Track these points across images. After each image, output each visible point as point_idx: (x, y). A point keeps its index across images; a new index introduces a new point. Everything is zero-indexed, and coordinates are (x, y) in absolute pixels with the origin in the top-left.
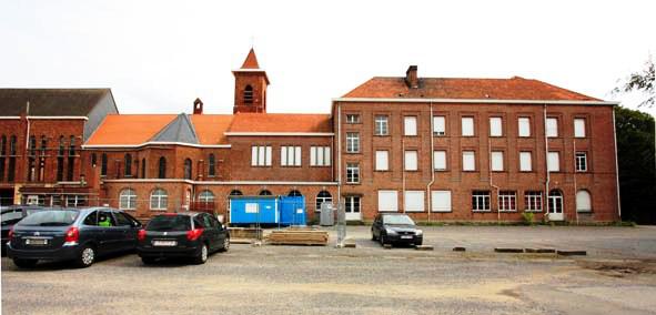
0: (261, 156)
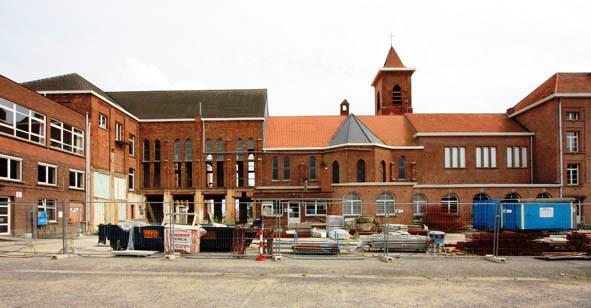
0: (454, 158)
